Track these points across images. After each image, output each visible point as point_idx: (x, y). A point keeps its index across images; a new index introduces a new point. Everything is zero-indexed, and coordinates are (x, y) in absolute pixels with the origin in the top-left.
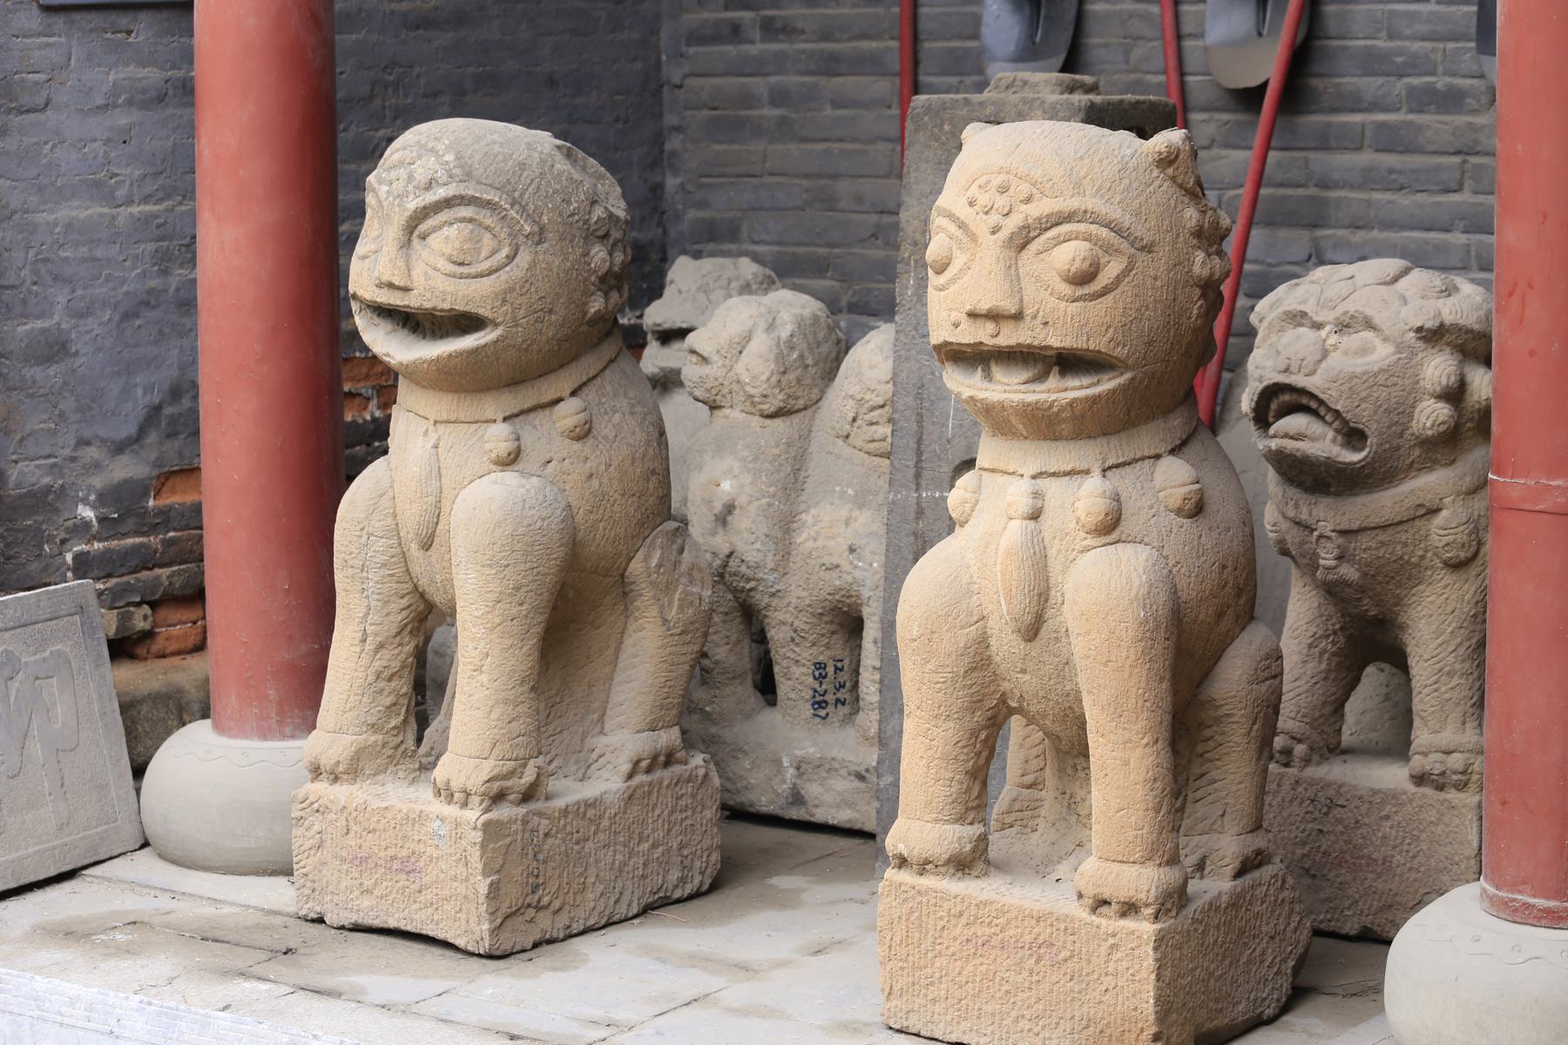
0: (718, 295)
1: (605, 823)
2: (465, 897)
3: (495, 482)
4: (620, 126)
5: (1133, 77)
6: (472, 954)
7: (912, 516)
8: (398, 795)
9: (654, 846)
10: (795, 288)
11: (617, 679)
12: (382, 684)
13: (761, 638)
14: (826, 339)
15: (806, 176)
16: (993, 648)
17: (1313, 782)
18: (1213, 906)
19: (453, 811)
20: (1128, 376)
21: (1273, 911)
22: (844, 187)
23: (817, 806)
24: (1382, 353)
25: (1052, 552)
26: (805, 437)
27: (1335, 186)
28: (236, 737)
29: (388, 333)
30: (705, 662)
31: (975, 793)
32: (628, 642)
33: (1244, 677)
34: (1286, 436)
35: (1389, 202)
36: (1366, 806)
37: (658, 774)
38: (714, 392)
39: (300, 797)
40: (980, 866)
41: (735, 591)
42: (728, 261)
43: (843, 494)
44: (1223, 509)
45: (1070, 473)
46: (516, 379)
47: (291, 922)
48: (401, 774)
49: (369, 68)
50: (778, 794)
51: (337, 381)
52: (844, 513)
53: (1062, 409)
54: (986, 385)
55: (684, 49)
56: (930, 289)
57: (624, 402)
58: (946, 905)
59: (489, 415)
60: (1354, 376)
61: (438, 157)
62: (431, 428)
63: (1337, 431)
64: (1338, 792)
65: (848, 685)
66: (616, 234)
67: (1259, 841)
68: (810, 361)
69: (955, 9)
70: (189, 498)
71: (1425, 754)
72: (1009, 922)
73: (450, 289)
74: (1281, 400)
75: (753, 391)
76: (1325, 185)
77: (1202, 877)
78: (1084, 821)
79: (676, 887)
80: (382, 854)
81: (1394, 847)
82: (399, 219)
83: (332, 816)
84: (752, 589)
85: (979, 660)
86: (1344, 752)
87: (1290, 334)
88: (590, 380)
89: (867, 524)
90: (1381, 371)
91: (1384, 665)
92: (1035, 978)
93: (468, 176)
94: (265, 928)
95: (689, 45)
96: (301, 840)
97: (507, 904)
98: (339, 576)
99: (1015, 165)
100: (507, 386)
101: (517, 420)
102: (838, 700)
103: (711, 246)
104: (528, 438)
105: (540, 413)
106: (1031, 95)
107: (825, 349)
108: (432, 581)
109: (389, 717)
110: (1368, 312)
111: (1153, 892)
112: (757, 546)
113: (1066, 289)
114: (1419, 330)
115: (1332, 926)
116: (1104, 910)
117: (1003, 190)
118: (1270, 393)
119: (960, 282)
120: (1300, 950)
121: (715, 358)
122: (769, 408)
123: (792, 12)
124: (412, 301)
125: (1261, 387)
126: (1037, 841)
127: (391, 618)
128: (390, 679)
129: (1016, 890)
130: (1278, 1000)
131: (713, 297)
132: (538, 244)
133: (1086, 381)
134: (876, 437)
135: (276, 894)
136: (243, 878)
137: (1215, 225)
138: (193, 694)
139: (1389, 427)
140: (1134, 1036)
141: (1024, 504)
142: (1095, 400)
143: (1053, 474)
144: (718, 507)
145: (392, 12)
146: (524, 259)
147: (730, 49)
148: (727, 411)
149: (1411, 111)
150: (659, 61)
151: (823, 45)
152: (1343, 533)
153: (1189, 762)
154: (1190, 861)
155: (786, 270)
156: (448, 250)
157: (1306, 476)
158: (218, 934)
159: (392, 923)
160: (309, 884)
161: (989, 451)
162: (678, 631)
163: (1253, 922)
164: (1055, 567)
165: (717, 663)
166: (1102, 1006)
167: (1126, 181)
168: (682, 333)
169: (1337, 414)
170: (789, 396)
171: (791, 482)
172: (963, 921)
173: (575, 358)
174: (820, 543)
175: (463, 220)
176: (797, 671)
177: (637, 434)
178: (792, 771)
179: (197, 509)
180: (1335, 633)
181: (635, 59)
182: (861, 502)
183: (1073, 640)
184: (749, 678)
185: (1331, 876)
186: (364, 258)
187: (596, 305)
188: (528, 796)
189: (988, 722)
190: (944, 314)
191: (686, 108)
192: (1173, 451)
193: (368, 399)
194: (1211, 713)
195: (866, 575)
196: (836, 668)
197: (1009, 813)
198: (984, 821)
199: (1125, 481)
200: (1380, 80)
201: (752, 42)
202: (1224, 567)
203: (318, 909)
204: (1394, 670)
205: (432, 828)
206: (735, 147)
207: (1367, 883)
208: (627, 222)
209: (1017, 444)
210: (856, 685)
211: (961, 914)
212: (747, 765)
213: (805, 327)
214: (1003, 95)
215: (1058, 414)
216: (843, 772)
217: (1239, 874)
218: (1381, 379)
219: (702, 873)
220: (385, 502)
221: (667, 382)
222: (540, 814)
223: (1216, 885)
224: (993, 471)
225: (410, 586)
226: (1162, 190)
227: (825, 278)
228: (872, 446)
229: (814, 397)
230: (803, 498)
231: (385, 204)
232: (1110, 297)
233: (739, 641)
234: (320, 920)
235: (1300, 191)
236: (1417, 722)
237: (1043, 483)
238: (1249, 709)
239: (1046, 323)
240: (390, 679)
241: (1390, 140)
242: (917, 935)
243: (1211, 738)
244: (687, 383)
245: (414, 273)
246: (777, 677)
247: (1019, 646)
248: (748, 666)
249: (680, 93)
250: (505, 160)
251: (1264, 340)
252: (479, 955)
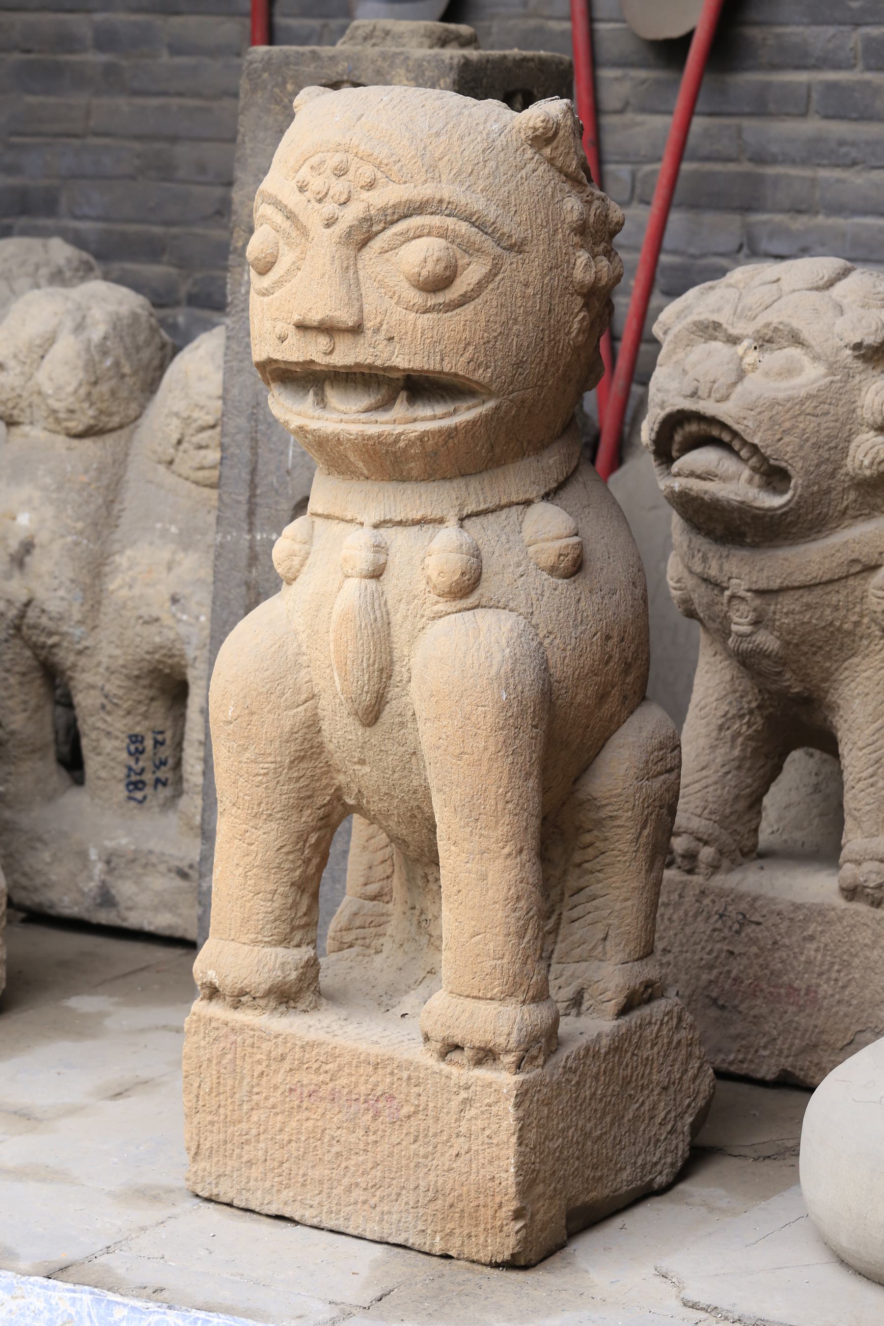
0: (22, 283)
5: (532, 23)
7: (243, 563)
14: (147, 343)
15: (139, 138)
16: (326, 734)
17: (722, 894)
18: (590, 1052)
20: (491, 404)
21: (666, 1056)
22: (183, 152)
23: (130, 909)
24: (811, 375)
25: (396, 619)
26: (121, 462)
27: (773, 161)
31: (303, 908)
33: (632, 772)
34: (692, 474)
35: (838, 181)
36: (786, 923)
40: (309, 997)
41: (35, 648)
43: (164, 533)
44: (609, 565)
50: (83, 894)
52: (165, 555)
53: (411, 444)
54: (318, 412)
56: (253, 295)
58: (265, 1046)
60: (775, 403)
63: (754, 469)
64: (752, 906)
67: (650, 971)
68: (127, 369)
71: (858, 863)
72: (340, 1068)
74: (688, 430)
75: (57, 405)
76: (760, 159)
77: (579, 1014)
78: (434, 943)
81: (820, 974)
84: (54, 646)
85: (308, 748)
86: (762, 856)
87: (701, 349)
89: (193, 568)
90: (809, 396)
91: (811, 750)
92: (372, 1138)
99: (355, 142)
102: (158, 781)
106: (394, 49)
107: (146, 354)
110: (796, 324)
111: (514, 1037)
112: (61, 593)
113: (416, 297)
114: (857, 346)
115: (744, 1069)
116: (455, 1056)
117: (341, 172)
118: (675, 421)
119: (288, 285)
120: (701, 1103)
122: (77, 426)
125: (662, 414)
126: (382, 965)
129: (351, 1029)
130: (673, 1165)
133: (440, 409)
134: (206, 463)
137: (604, 218)
139: (818, 466)
140: (490, 1212)
141: (363, 560)
142: (450, 434)
143: (400, 523)
144: (14, 545)
148: (26, 429)
149: (869, 68)
152: (760, 593)
153: (565, 872)
154: (561, 995)
155: (107, 254)
157: (719, 525)
161: (324, 493)
163: (640, 1069)
164: (400, 635)
165: (12, 733)
166: (452, 1175)
167: (492, 164)
169: (755, 449)
170: (101, 412)
171: (103, 517)
172: (286, 1065)
174: (136, 591)
176: (108, 745)
180: (751, 712)
182: (185, 542)
183: (420, 725)
185: (743, 1007)
189: (320, 824)
190: (268, 324)
192: (547, 497)
194: (593, 815)
195: (189, 626)
197: (348, 929)
198: (313, 942)
199: (486, 532)
200: (831, 30)
202: (608, 638)
204: (825, 756)
207: (787, 1018)
209: (357, 486)
210: (178, 764)
211: (283, 1058)
213: (120, 328)
214: (359, 48)
215: (405, 450)
216: (162, 868)
217: (624, 1010)
218: (809, 406)
223: (596, 1025)
224: (328, 517)
226: (537, 174)
228: (201, 474)
229: (132, 413)
232: (470, 307)
233: (38, 708)
235: (732, 167)
236: (849, 824)
237: (388, 534)
238: (637, 810)
239: (391, 339)
241: (843, 105)
242: (230, 1082)
243: (591, 844)
251: (669, 356)
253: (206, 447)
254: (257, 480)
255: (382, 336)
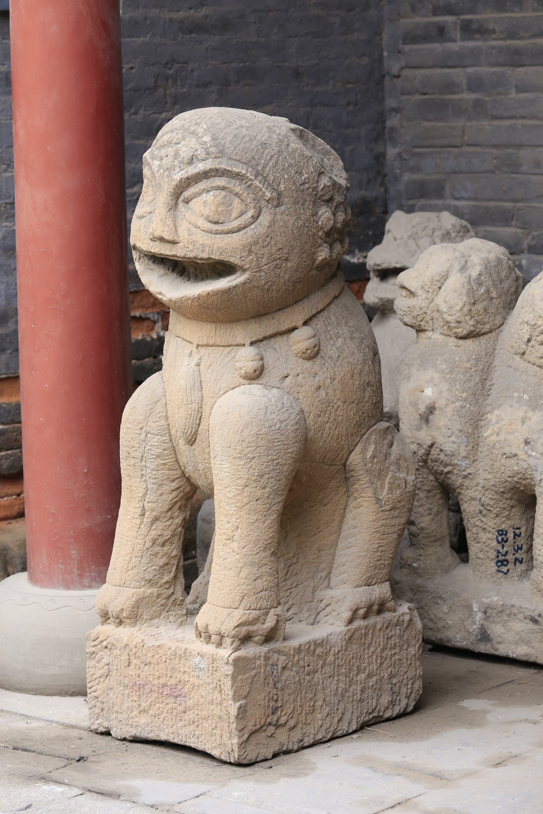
0: (425, 241)
1: (331, 658)
2: (220, 717)
3: (244, 393)
4: (351, 108)
6: (225, 763)
8: (169, 635)
9: (369, 676)
10: (486, 237)
11: (341, 545)
12: (157, 549)
13: (456, 509)
15: (496, 146)
19: (210, 649)
22: (525, 154)
23: (500, 643)
26: (491, 354)
29: (161, 276)
30: (413, 528)
32: (349, 516)
37: (372, 620)
38: (419, 319)
39: (93, 636)
41: (436, 474)
42: (432, 215)
46: (260, 313)
47: (85, 734)
48: (172, 619)
49: (153, 64)
50: (469, 633)
51: (124, 308)
55: (401, 46)
57: (346, 330)
59: (239, 340)
61: (198, 138)
62: (195, 350)
65: (525, 547)
66: (338, 198)
70: (13, 400)
73: (208, 242)
75: (449, 318)
79: (387, 708)
80: (156, 682)
82: (168, 187)
83: (117, 652)
88: (318, 313)
93: (221, 154)
94: (64, 739)
95: (404, 44)
96: (94, 670)
97: (252, 723)
98: (123, 465)
100: (254, 317)
101: (261, 344)
102: (516, 560)
103: (422, 202)
104: (269, 360)
105: (279, 339)
107: (506, 284)
108: (196, 469)
109: (162, 574)
112: (453, 438)
121: (420, 292)
122: (462, 331)
123: (486, 16)
124: (178, 252)
127: (164, 497)
128: (163, 545)
131: (420, 243)
132: (277, 207)
135: (73, 711)
136: (49, 698)
138: (15, 551)
144: (422, 408)
145: (171, 20)
146: (265, 218)
147: (436, 46)
148: (430, 334)
150: (381, 56)
151: (509, 42)
155: (478, 221)
156: (206, 212)
158: (27, 745)
159: (163, 737)
160: (98, 705)
162: (388, 508)
165: (422, 529)
168: (396, 271)
170: (478, 322)
171: (480, 389)
173: (306, 295)
174: (502, 437)
175: (218, 188)
176: (484, 536)
177: (354, 355)
178: (480, 615)
179: (18, 407)
181: (363, 55)
184: (447, 541)
186: (141, 217)
187: (323, 254)
188: (269, 637)
191: (403, 94)
193: (155, 322)
196: (515, 534)
201: (455, 41)
203: (106, 724)
205: (194, 660)
206: (440, 124)
208: (347, 188)
210: (530, 548)
212: (445, 609)
216: (521, 616)
219: (408, 697)
220: (159, 408)
221: (383, 310)
222: (279, 652)
225: (178, 473)
227: (511, 226)
229: (498, 323)
230: (488, 402)
231: (157, 175)
233: (438, 513)
234: (107, 733)
240: (163, 545)
244: (399, 312)
245: (180, 230)
246: (469, 541)
248: (446, 532)
249: (398, 82)
250: (251, 141)
252: (230, 764)
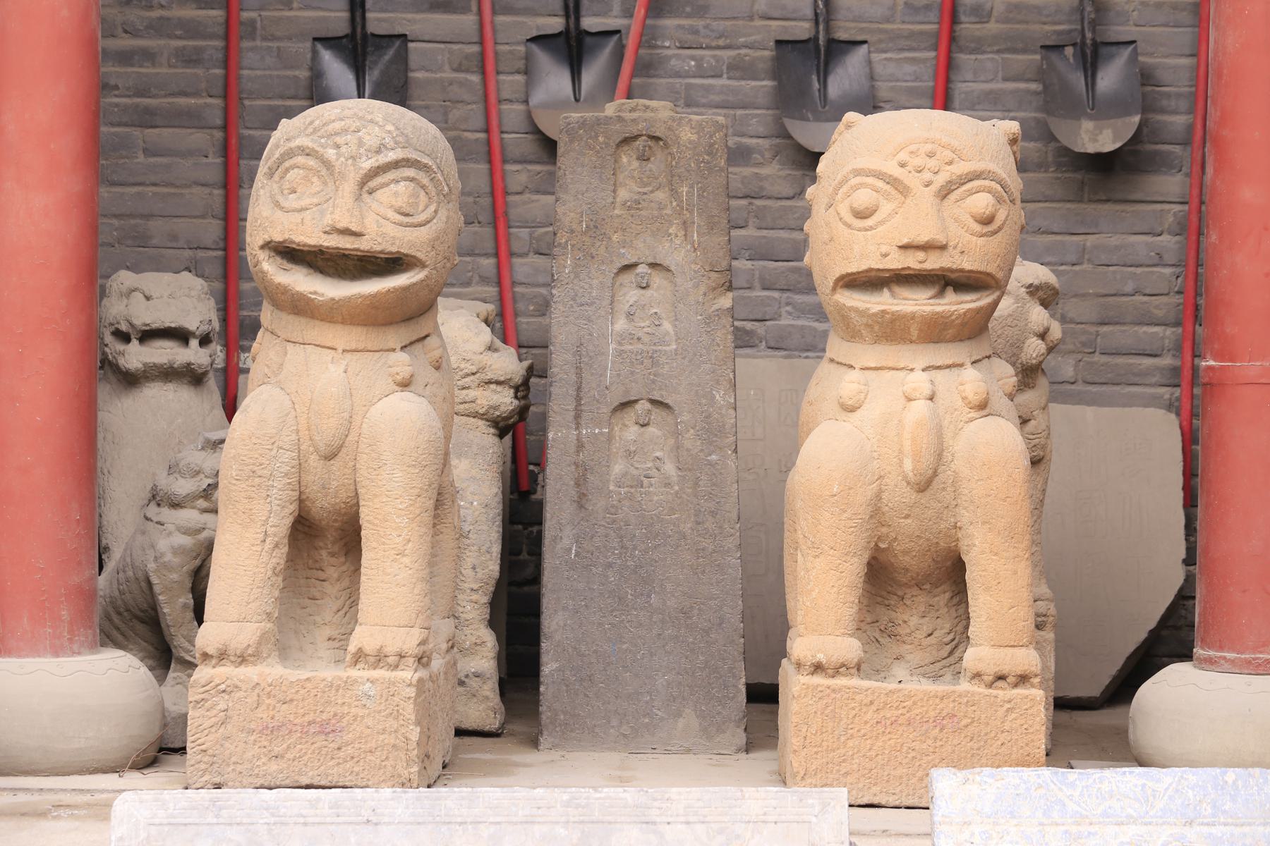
7: (573, 449)
15: (115, 216)
22: (156, 225)
25: (946, 423)
28: (27, 656)
45: (949, 367)
58: (858, 697)
59: (391, 345)
69: (276, 73)
72: (915, 703)
73: (398, 235)
82: (353, 177)
92: (939, 743)
113: (977, 228)
117: (931, 155)
172: (874, 708)
232: (1000, 234)
247: (910, 496)
253: (468, 388)
254: (582, 394)
255: (959, 249)
